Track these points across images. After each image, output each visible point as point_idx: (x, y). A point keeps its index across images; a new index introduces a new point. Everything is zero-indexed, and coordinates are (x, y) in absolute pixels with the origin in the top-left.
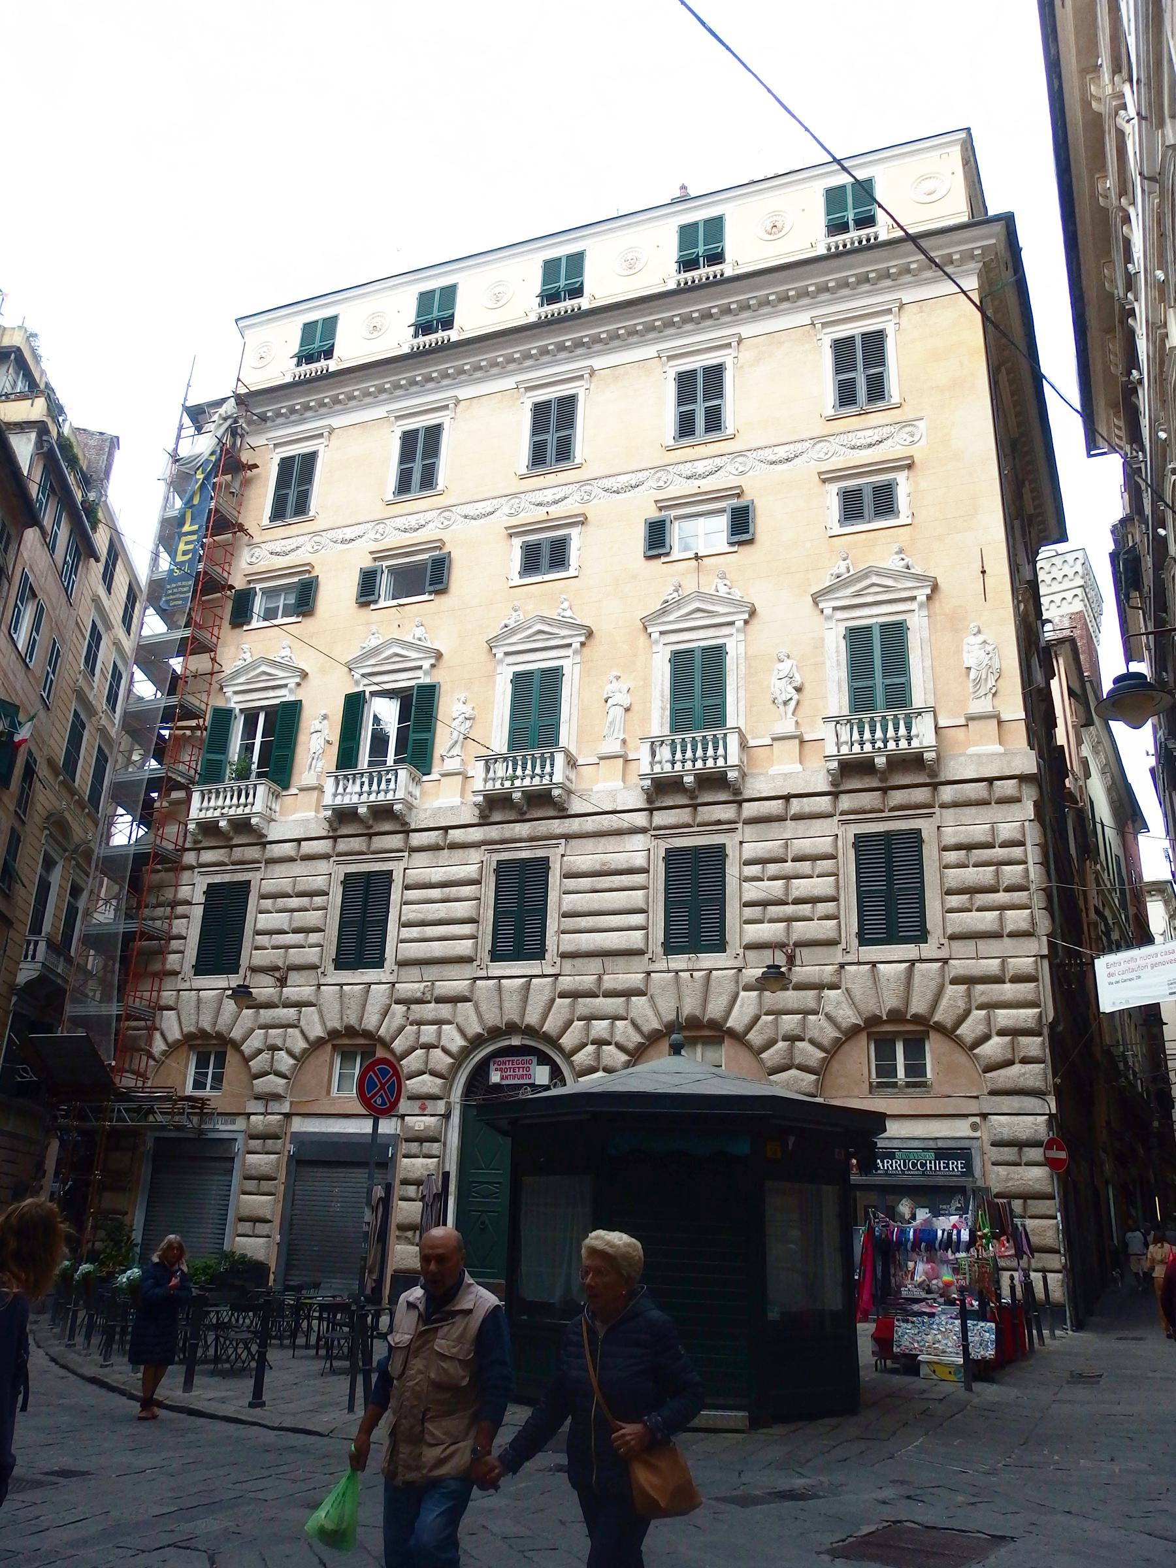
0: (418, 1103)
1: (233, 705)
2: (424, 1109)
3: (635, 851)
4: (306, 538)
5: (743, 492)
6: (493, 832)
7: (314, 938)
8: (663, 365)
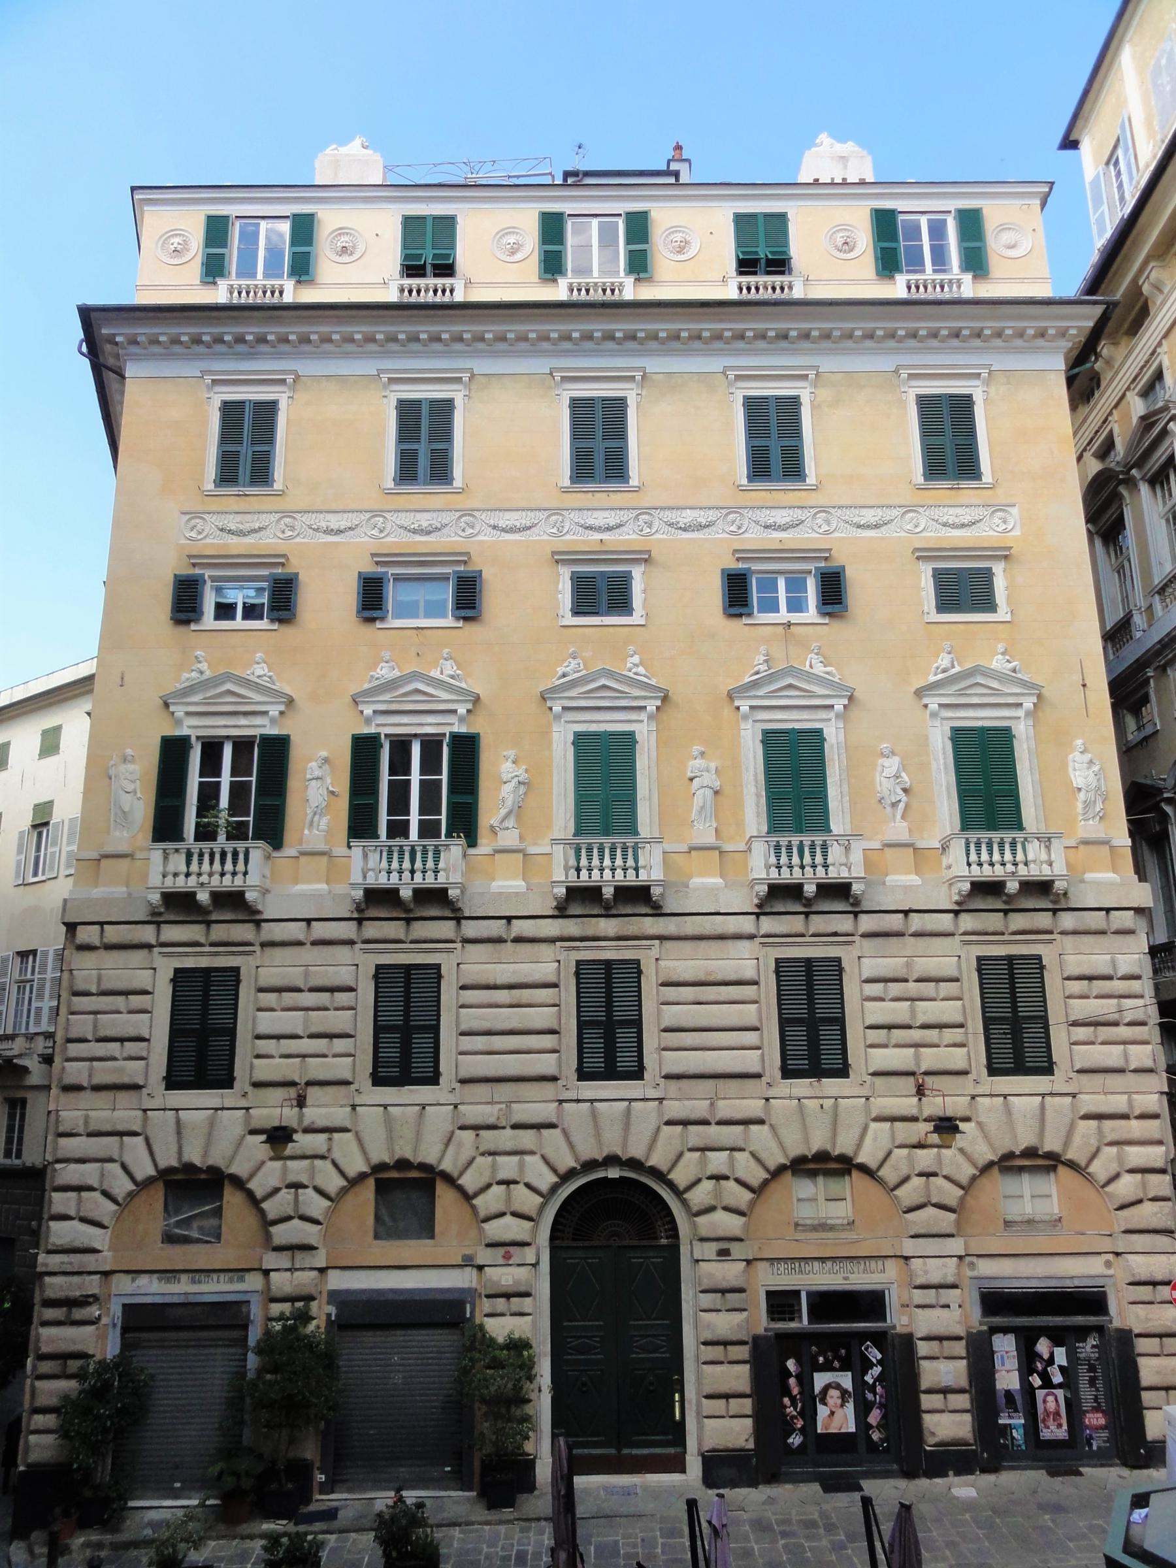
0: (501, 1251)
4: (274, 517)
5: (470, 558)
6: (571, 927)
7: (340, 1045)
8: (730, 384)
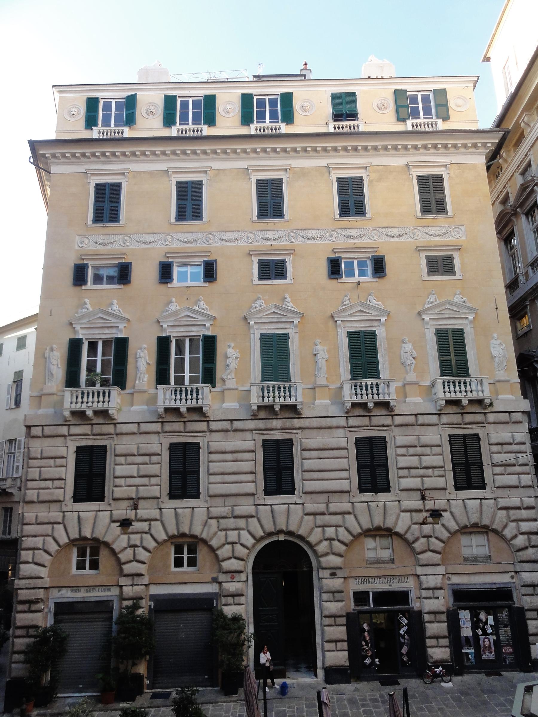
0: (229, 575)
1: (81, 337)
2: (234, 578)
3: (247, 442)
6: (260, 424)
7: (154, 480)
